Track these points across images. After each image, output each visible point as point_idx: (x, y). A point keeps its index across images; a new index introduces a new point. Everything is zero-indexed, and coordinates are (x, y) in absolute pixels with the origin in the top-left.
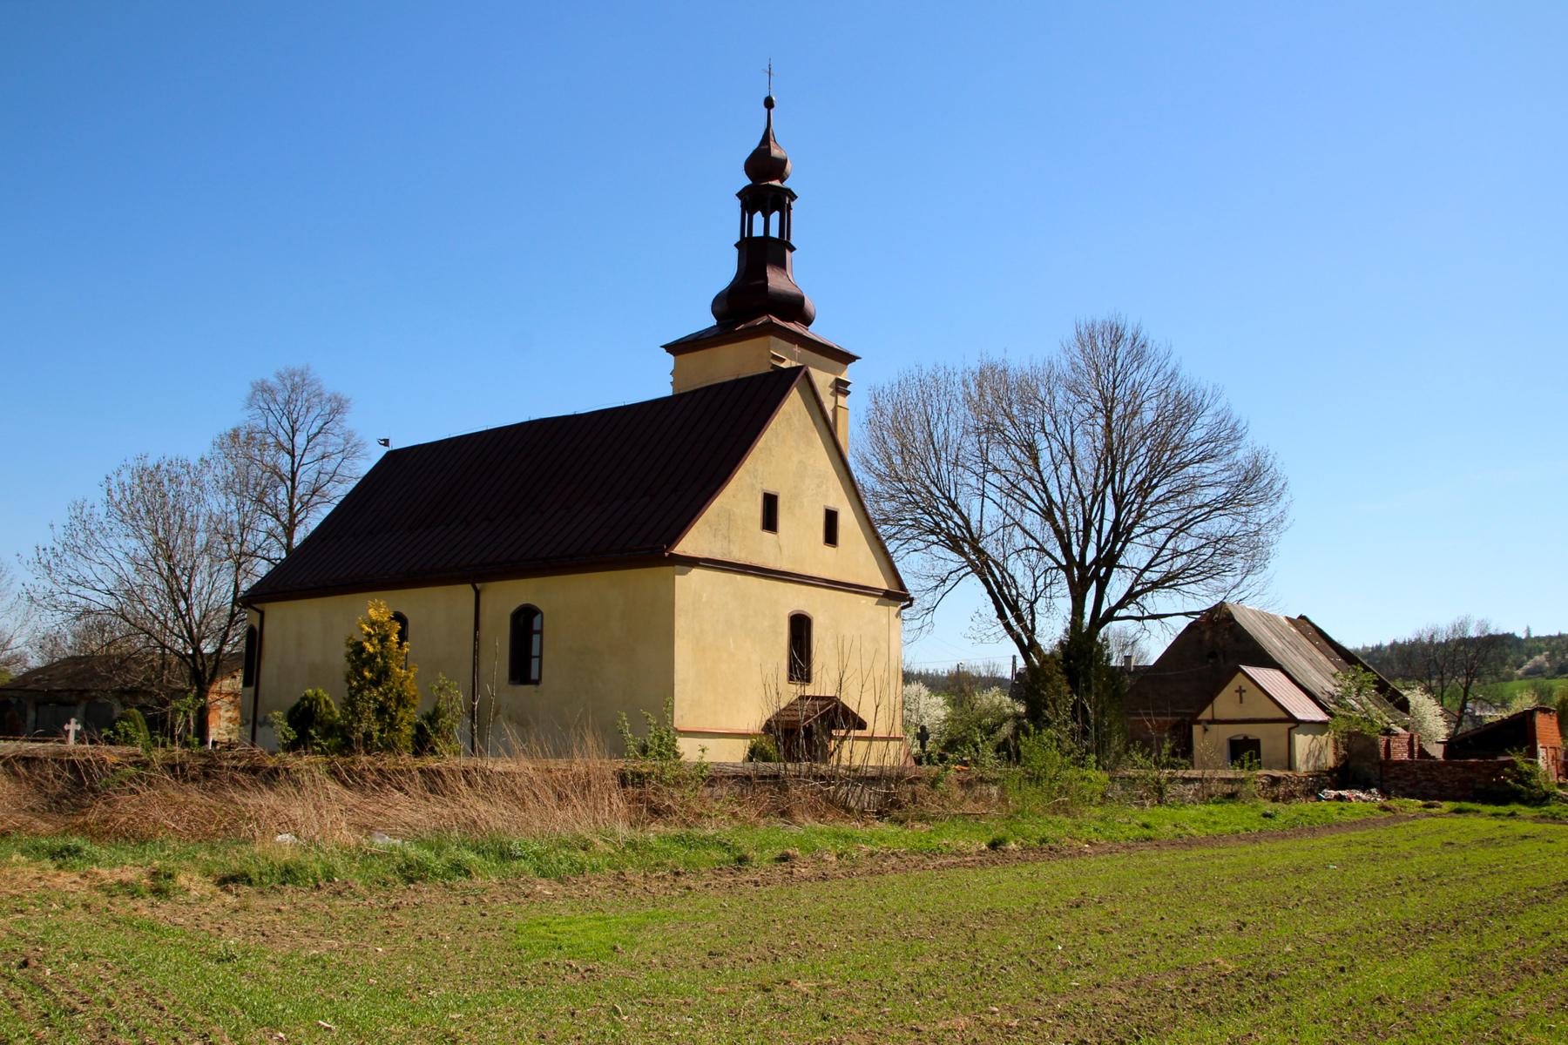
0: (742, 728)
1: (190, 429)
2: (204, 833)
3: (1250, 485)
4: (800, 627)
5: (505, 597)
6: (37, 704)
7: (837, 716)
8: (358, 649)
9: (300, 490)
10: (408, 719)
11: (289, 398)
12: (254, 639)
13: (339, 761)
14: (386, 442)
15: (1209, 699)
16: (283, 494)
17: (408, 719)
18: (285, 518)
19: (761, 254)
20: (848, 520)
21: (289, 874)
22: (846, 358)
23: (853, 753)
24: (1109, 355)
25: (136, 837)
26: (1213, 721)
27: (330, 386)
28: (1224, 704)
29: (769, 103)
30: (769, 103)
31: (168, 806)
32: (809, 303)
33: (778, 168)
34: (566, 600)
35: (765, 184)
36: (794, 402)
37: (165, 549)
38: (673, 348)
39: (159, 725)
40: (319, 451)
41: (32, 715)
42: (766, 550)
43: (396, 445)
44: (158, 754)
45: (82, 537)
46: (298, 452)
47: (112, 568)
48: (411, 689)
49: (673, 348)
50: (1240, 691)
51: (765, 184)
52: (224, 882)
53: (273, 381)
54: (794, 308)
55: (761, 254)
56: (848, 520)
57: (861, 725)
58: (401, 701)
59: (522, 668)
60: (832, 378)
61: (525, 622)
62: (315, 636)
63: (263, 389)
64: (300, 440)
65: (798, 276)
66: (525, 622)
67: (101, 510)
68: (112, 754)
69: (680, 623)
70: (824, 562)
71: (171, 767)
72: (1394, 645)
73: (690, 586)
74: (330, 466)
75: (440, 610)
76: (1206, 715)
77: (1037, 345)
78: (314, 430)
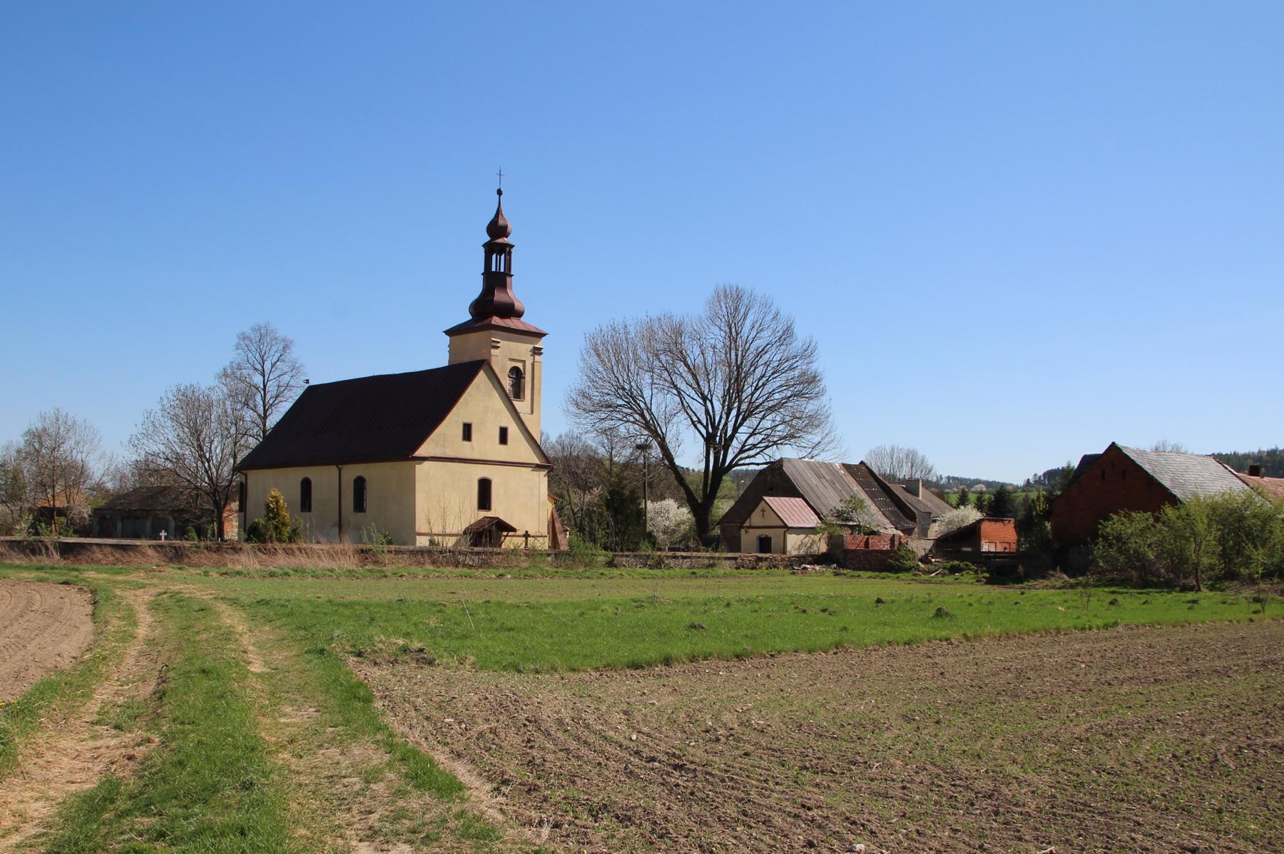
0: (455, 531)
1: (204, 367)
2: (217, 564)
3: (807, 384)
4: (485, 487)
5: (352, 472)
6: (123, 519)
7: (503, 527)
8: (268, 506)
9: (268, 397)
10: (287, 531)
11: (260, 344)
12: (243, 488)
13: (261, 546)
14: (307, 381)
15: (749, 515)
16: (258, 398)
17: (287, 531)
18: (262, 413)
19: (495, 280)
20: (514, 431)
21: (239, 573)
22: (540, 335)
23: (509, 542)
24: (732, 308)
25: (197, 566)
26: (750, 527)
27: (281, 334)
28: (756, 518)
29: (500, 192)
30: (500, 192)
31: (207, 558)
32: (517, 306)
33: (504, 231)
34: (377, 474)
35: (497, 240)
36: (481, 377)
37: (196, 432)
38: (448, 332)
39: (201, 533)
40: (278, 373)
41: (119, 525)
42: (466, 450)
43: (312, 383)
44: (202, 544)
45: (152, 429)
46: (267, 372)
47: (165, 442)
48: (287, 520)
49: (448, 332)
50: (763, 511)
51: (497, 240)
52: (222, 574)
53: (249, 332)
54: (510, 311)
55: (495, 280)
56: (514, 431)
57: (514, 530)
58: (284, 524)
59: (359, 505)
60: (531, 346)
61: (360, 484)
62: (276, 487)
63: (244, 337)
64: (268, 366)
65: (517, 292)
66: (360, 484)
67: (160, 413)
68: (187, 544)
69: (418, 487)
70: (502, 453)
71: (207, 548)
72: (1088, 461)
73: (422, 470)
74: (286, 378)
75: (324, 478)
76: (747, 524)
77: (690, 305)
78: (275, 359)
